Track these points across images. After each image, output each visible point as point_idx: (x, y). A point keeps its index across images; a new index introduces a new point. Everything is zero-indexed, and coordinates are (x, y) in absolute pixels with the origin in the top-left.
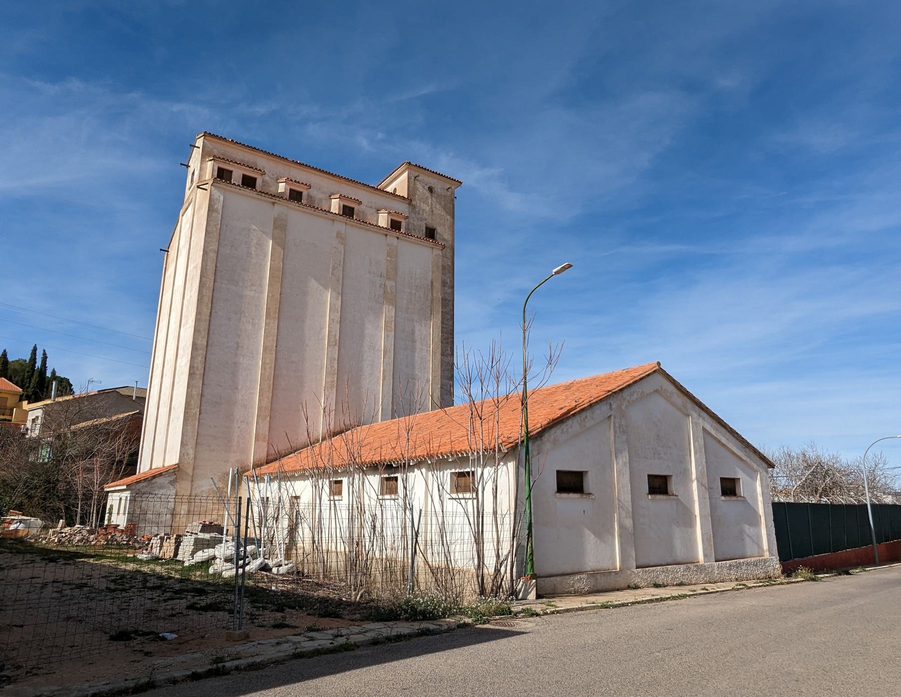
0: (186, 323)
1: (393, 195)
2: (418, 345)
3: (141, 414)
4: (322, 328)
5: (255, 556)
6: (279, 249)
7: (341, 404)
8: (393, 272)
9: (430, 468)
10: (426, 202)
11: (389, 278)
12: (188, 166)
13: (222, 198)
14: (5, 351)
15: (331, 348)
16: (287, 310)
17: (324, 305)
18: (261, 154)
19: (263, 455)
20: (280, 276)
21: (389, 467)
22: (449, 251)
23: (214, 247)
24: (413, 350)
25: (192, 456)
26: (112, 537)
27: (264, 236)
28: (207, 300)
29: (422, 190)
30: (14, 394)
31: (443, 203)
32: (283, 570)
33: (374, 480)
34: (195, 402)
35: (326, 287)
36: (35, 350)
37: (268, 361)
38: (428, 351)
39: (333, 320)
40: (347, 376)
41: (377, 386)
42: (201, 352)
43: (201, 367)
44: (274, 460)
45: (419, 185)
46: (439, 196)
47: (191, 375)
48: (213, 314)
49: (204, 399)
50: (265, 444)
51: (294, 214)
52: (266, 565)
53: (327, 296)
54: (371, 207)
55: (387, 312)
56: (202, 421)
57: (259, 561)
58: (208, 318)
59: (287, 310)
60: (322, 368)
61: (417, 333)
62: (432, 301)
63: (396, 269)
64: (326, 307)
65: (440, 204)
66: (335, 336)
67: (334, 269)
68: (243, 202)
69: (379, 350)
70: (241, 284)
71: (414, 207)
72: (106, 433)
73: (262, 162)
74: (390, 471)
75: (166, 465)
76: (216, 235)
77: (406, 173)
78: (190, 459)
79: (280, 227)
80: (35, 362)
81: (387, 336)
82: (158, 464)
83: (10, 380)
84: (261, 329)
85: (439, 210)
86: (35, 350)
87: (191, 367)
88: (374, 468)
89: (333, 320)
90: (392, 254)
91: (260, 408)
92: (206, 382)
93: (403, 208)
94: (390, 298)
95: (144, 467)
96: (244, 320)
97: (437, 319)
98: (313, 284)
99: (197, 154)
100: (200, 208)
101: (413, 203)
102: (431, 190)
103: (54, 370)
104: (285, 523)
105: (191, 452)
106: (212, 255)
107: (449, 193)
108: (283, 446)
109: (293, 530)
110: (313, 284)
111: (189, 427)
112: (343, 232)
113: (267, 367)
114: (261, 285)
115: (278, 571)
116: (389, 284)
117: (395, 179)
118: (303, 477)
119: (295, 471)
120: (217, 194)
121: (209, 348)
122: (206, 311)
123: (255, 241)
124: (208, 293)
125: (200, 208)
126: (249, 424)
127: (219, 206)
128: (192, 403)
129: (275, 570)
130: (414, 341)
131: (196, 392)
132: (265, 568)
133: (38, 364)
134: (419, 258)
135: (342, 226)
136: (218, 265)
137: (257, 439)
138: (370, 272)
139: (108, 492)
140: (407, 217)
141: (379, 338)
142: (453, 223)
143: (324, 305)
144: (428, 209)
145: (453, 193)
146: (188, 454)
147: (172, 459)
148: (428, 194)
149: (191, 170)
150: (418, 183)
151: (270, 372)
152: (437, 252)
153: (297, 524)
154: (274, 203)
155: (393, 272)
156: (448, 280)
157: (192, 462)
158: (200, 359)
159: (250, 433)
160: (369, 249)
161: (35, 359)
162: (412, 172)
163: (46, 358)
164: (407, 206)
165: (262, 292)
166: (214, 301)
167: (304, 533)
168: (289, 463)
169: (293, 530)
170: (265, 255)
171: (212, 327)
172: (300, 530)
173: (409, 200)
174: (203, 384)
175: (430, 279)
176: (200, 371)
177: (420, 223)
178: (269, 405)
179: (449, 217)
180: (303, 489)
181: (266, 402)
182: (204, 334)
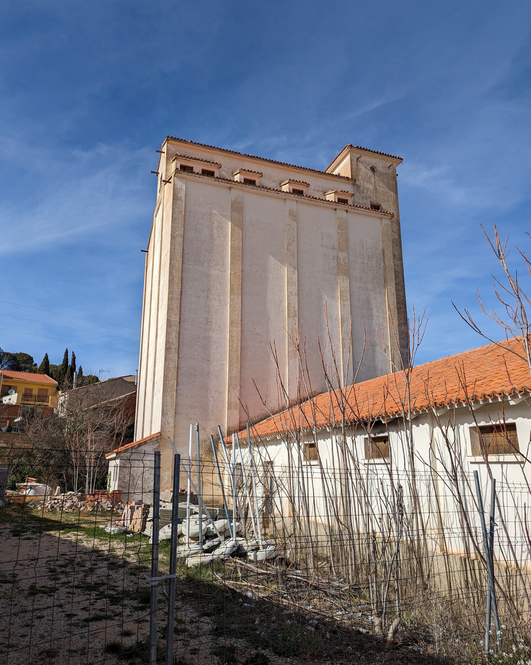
0: (162, 306)
1: (338, 176)
2: (375, 313)
3: (136, 393)
4: (281, 302)
5: (226, 534)
6: (238, 230)
7: (305, 370)
8: (344, 244)
9: (435, 421)
10: (369, 182)
11: (341, 250)
12: (158, 173)
13: (184, 186)
14: (46, 354)
15: (291, 320)
16: (249, 286)
17: (282, 280)
18: (218, 152)
19: (235, 423)
20: (240, 254)
21: (378, 425)
22: (395, 220)
23: (180, 231)
24: (370, 317)
25: (172, 425)
26: (98, 503)
27: (224, 219)
28: (177, 280)
29: (364, 171)
30: (52, 386)
31: (386, 182)
32: (261, 555)
33: (359, 443)
34: (173, 374)
35: (282, 262)
36: (67, 352)
37: (235, 334)
38: (384, 318)
39: (291, 293)
40: (308, 346)
41: (339, 355)
42: (175, 328)
43: (175, 341)
44: (249, 428)
45: (361, 166)
46: (381, 174)
47: (168, 349)
48: (183, 294)
49: (180, 372)
50: (237, 412)
51: (251, 198)
52: (240, 547)
53: (284, 271)
54: (318, 191)
55: (343, 283)
56: (179, 392)
57: (230, 543)
58: (179, 296)
59: (249, 286)
60: (284, 338)
61: (373, 301)
62: (385, 269)
63: (347, 240)
64: (284, 282)
65: (383, 182)
66: (294, 308)
67: (289, 245)
68: (203, 190)
69: (337, 319)
70: (206, 264)
71: (358, 187)
72: (110, 412)
73: (218, 158)
74: (378, 429)
75: (153, 433)
76: (181, 220)
77: (348, 157)
78: (170, 429)
79: (237, 210)
80: (67, 362)
81: (343, 306)
82: (147, 435)
83: (52, 377)
84: (226, 305)
85: (382, 188)
86: (67, 352)
87: (167, 342)
88: (357, 426)
89: (291, 293)
90: (343, 227)
91: (230, 378)
92: (180, 356)
93: (348, 188)
94: (343, 269)
95: (138, 437)
96: (211, 297)
97: (391, 287)
98: (272, 261)
99: (164, 156)
100: (167, 202)
101: (357, 183)
102: (373, 169)
103: (81, 367)
104: (259, 491)
105: (171, 420)
106: (179, 240)
107: (390, 171)
108: (254, 414)
109: (268, 500)
110: (272, 261)
111: (168, 398)
112: (295, 210)
113: (235, 339)
114: (224, 265)
115: (256, 556)
116: (341, 255)
117: (338, 165)
118: (275, 442)
119: (267, 435)
120: (181, 185)
121: (182, 324)
122: (177, 290)
123: (216, 224)
124: (177, 274)
125: (167, 202)
126: (221, 393)
127: (182, 195)
128: (170, 375)
129: (251, 556)
130: (370, 309)
131: (173, 365)
132: (239, 552)
133: (70, 363)
134: (368, 230)
135: (293, 204)
136: (185, 248)
137: (229, 408)
138: (322, 246)
139: (109, 460)
140: (353, 195)
141: (337, 309)
142: (397, 198)
143: (282, 280)
144: (371, 187)
145: (394, 170)
146: (168, 423)
147: (156, 429)
148: (370, 173)
149: (160, 176)
150: (360, 164)
151: (237, 344)
152: (386, 221)
153: (272, 493)
154: (230, 188)
155: (344, 244)
156: (396, 253)
157: (172, 430)
158: (174, 334)
159: (223, 401)
160: (320, 224)
161: (67, 359)
162: (354, 154)
163: (75, 358)
164: (351, 186)
165: (225, 271)
166: (184, 281)
167: (282, 504)
168: (262, 428)
169: (268, 500)
170: (225, 237)
171: (183, 305)
172: (277, 500)
173: (353, 180)
174: (178, 357)
175: (381, 248)
176: (175, 346)
177: (365, 201)
178: (238, 374)
179: (392, 193)
180: (279, 454)
181: (236, 373)
182: (177, 311)
